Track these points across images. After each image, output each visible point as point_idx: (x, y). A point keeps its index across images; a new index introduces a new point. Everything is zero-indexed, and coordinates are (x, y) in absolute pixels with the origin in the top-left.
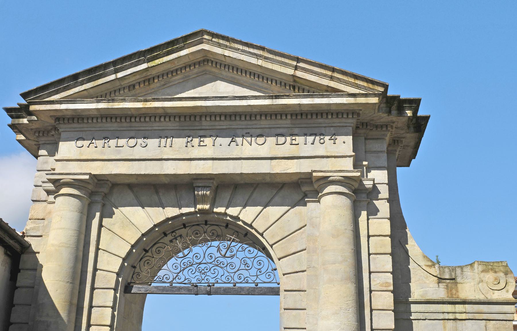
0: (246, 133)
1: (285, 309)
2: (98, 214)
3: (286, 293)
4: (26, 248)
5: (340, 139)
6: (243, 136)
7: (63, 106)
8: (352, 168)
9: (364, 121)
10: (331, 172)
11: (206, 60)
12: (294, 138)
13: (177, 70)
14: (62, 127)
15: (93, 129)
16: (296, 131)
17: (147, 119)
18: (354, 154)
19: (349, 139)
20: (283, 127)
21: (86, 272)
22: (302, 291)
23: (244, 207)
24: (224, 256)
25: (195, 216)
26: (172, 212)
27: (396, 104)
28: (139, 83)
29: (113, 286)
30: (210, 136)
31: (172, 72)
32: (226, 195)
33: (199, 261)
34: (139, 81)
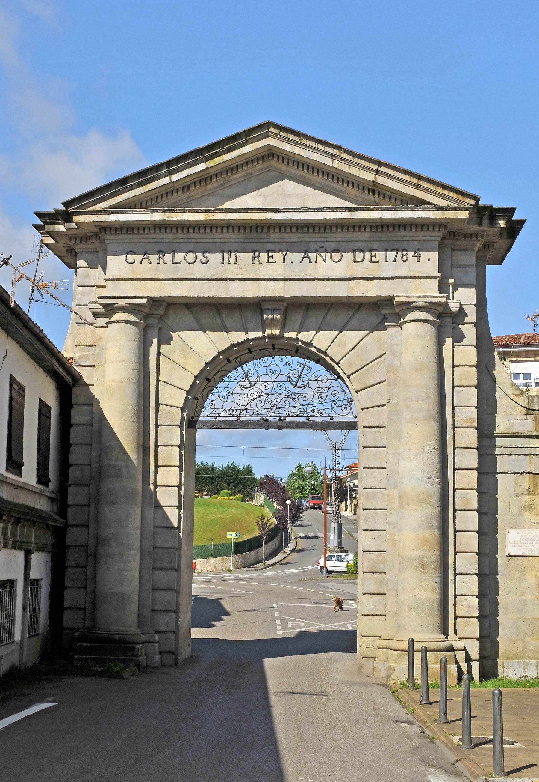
0: (320, 248)
1: (364, 447)
2: (155, 341)
3: (365, 429)
4: (77, 379)
5: (425, 255)
6: (317, 251)
7: (113, 218)
8: (437, 293)
9: (451, 230)
10: (415, 296)
11: (271, 153)
12: (373, 254)
13: (237, 167)
14: (109, 238)
15: (145, 241)
16: (376, 245)
17: (208, 230)
18: (439, 274)
19: (435, 256)
20: (362, 241)
21: (149, 408)
22: (382, 427)
23: (318, 332)
24: (295, 386)
25: (262, 341)
26: (237, 337)
27: (487, 214)
28: (195, 183)
29: (179, 423)
30: (280, 251)
31: (232, 169)
32: (296, 317)
33: (267, 392)
34: (194, 181)
